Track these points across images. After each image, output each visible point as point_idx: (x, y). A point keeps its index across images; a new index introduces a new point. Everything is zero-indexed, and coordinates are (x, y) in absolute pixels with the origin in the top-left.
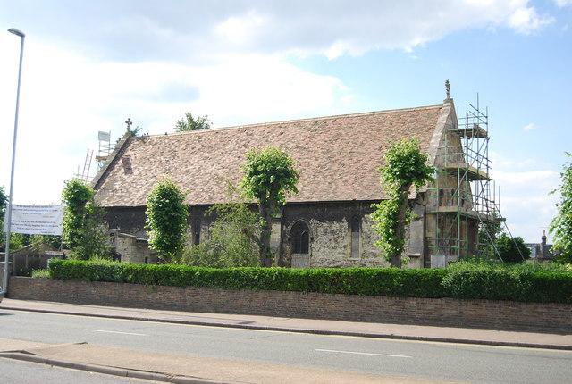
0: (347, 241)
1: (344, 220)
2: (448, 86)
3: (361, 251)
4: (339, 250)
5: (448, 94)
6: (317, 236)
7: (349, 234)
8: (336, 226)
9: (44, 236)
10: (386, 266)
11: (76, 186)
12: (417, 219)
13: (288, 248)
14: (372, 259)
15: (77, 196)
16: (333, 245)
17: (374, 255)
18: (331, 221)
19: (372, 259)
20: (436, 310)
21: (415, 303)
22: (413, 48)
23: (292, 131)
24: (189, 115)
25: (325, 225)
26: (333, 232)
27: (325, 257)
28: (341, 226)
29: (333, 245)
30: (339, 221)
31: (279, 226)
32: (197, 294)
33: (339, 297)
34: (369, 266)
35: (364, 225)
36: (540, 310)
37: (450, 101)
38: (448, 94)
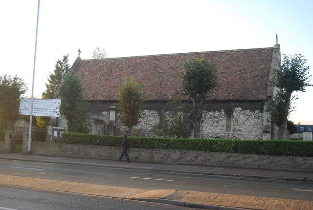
0: (224, 122)
1: (222, 110)
3: (232, 128)
4: (219, 128)
5: (277, 41)
6: (206, 119)
7: (225, 118)
8: (217, 114)
10: (97, 134)
14: (240, 133)
16: (216, 124)
17: (240, 131)
18: (214, 111)
21: (302, 159)
26: (215, 117)
27: (210, 131)
28: (220, 114)
29: (216, 124)
30: (219, 111)
32: (161, 153)
33: (254, 156)
35: (234, 113)
37: (278, 46)
38: (277, 41)
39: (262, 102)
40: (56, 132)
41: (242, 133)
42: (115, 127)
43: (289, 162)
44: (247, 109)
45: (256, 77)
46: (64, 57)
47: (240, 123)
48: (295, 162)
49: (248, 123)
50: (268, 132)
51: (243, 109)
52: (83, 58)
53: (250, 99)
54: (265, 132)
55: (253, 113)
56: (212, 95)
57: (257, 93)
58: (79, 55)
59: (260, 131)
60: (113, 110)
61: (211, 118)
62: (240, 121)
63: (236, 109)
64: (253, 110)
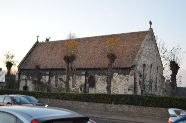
2: (151, 23)
5: (151, 26)
6: (98, 81)
11: (12, 64)
12: (132, 75)
13: (88, 85)
14: (116, 90)
17: (117, 89)
18: (102, 75)
20: (116, 108)
21: (109, 106)
22: (13, 89)
25: (101, 77)
31: (84, 77)
35: (114, 77)
36: (149, 110)
37: (151, 31)
38: (151, 26)
39: (129, 69)
41: (118, 90)
42: (47, 86)
43: (103, 108)
44: (121, 74)
45: (131, 52)
46: (47, 39)
47: (117, 83)
48: (106, 108)
49: (121, 84)
50: (131, 90)
51: (119, 74)
52: (40, 41)
53: (122, 67)
54: (129, 90)
55: (124, 77)
56: (115, 64)
57: (127, 63)
59: (125, 90)
60: (47, 75)
61: (101, 80)
62: (117, 82)
63: (115, 74)
64: (124, 74)
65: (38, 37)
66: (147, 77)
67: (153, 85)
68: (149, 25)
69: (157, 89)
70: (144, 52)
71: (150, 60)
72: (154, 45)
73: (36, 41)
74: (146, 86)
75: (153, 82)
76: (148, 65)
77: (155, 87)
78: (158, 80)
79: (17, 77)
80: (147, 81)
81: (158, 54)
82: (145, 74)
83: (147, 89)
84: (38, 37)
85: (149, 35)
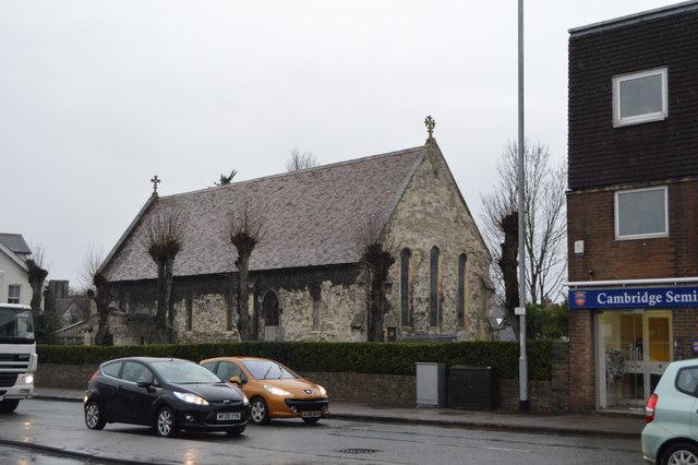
0: (310, 310)
4: (303, 322)
5: (430, 132)
8: (300, 295)
9: (535, 193)
14: (329, 332)
15: (99, 279)
16: (298, 317)
17: (331, 327)
19: (329, 332)
23: (349, 169)
24: (310, 154)
26: (298, 302)
28: (305, 295)
29: (298, 317)
34: (328, 339)
37: (431, 142)
38: (430, 132)
40: (576, 251)
44: (339, 283)
46: (159, 181)
52: (162, 193)
58: (155, 188)
62: (331, 307)
64: (347, 284)
65: (156, 181)
66: (418, 289)
67: (446, 310)
68: (426, 129)
69: (466, 323)
70: (403, 214)
71: (429, 237)
72: (443, 190)
73: (149, 195)
74: (417, 313)
75: (447, 300)
76: (423, 252)
77: (455, 316)
78: (467, 295)
79: (262, 321)
80: (419, 300)
81: (465, 215)
82: (410, 278)
83: (391, 319)
84: (156, 181)
85: (66, 282)
